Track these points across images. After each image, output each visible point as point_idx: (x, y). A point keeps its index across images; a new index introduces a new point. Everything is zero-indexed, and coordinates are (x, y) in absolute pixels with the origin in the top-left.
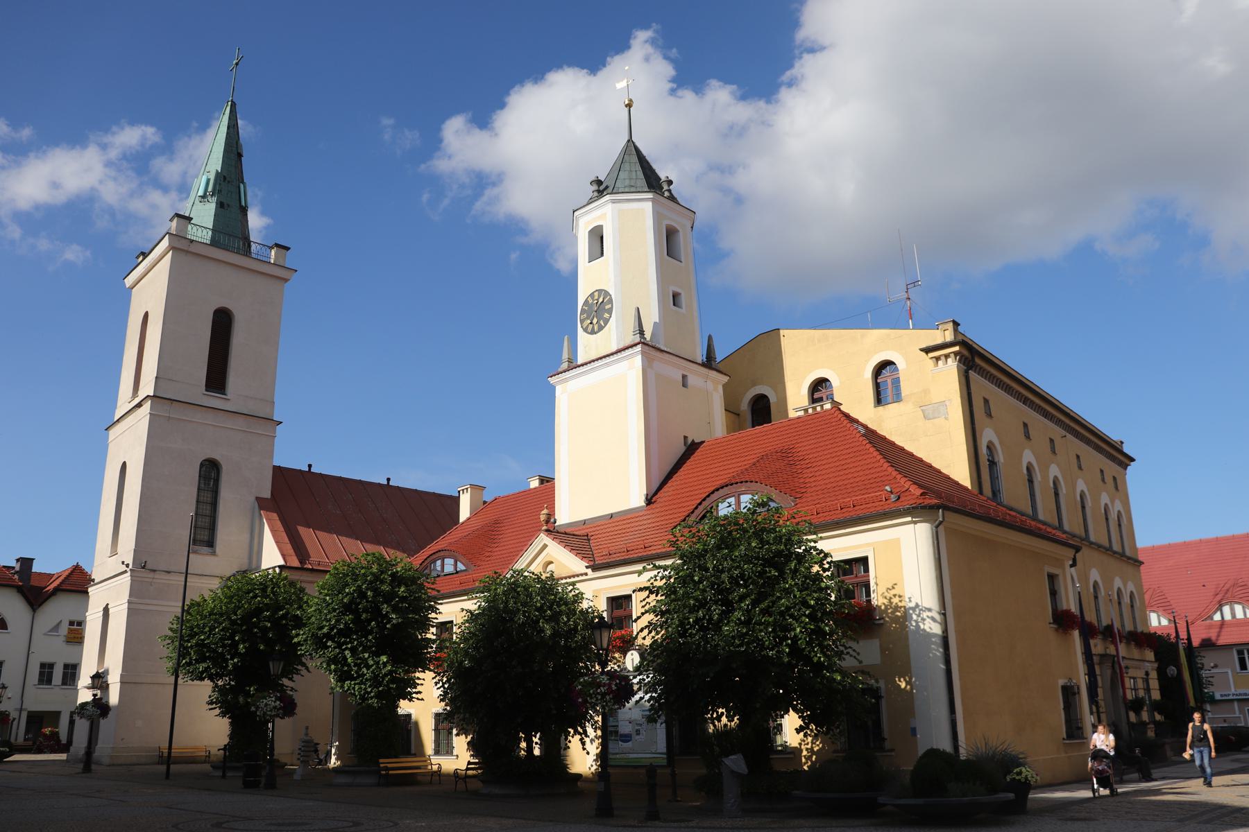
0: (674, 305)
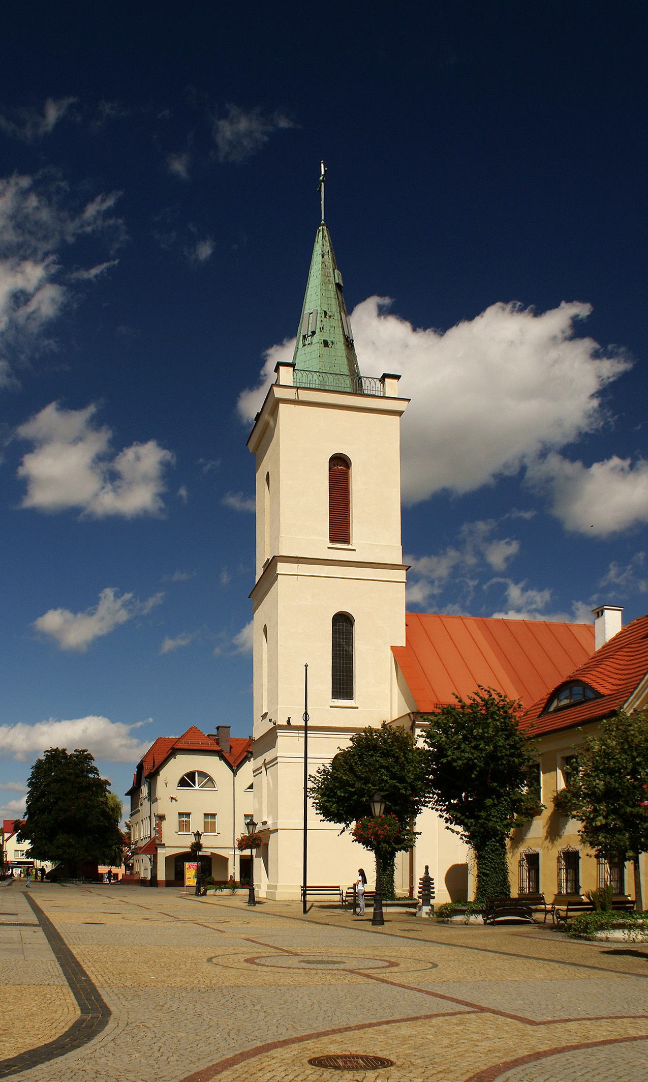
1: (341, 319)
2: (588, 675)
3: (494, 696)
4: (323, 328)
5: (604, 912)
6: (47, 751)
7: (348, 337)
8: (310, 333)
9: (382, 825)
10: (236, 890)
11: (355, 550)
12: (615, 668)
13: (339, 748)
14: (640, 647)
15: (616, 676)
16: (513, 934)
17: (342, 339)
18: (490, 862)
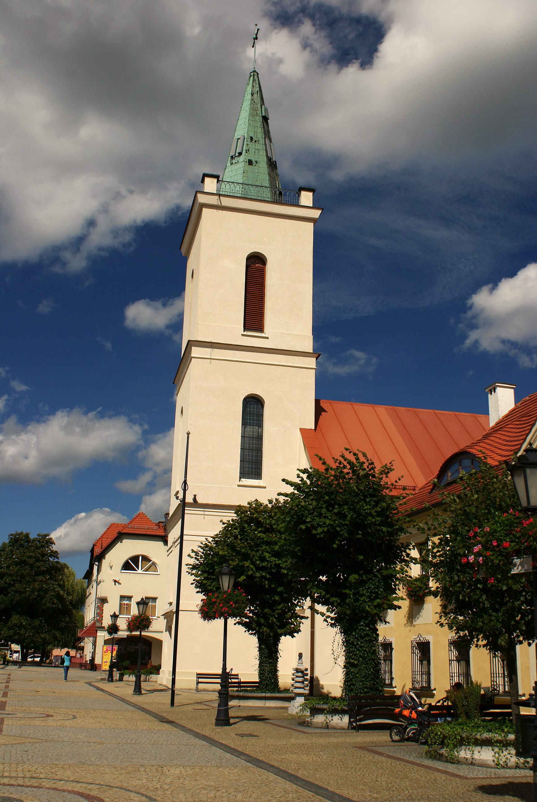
1: (265, 144)
2: (475, 447)
3: (362, 459)
4: (248, 150)
5: (468, 722)
6: (12, 535)
7: (271, 158)
8: (237, 154)
9: (228, 602)
10: (151, 675)
11: (267, 338)
12: (504, 440)
13: (221, 521)
14: (529, 419)
15: (504, 447)
16: (363, 748)
17: (265, 159)
18: (359, 650)
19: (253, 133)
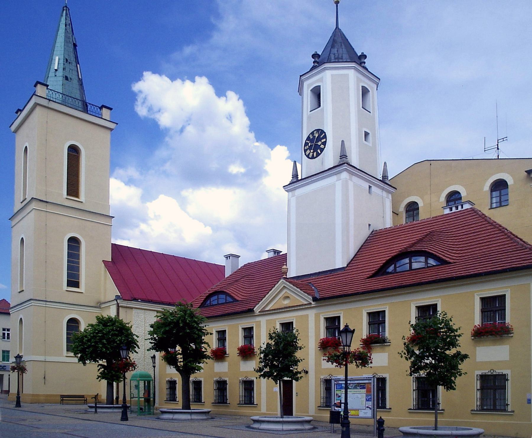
0: (365, 140)
19: (67, 56)
